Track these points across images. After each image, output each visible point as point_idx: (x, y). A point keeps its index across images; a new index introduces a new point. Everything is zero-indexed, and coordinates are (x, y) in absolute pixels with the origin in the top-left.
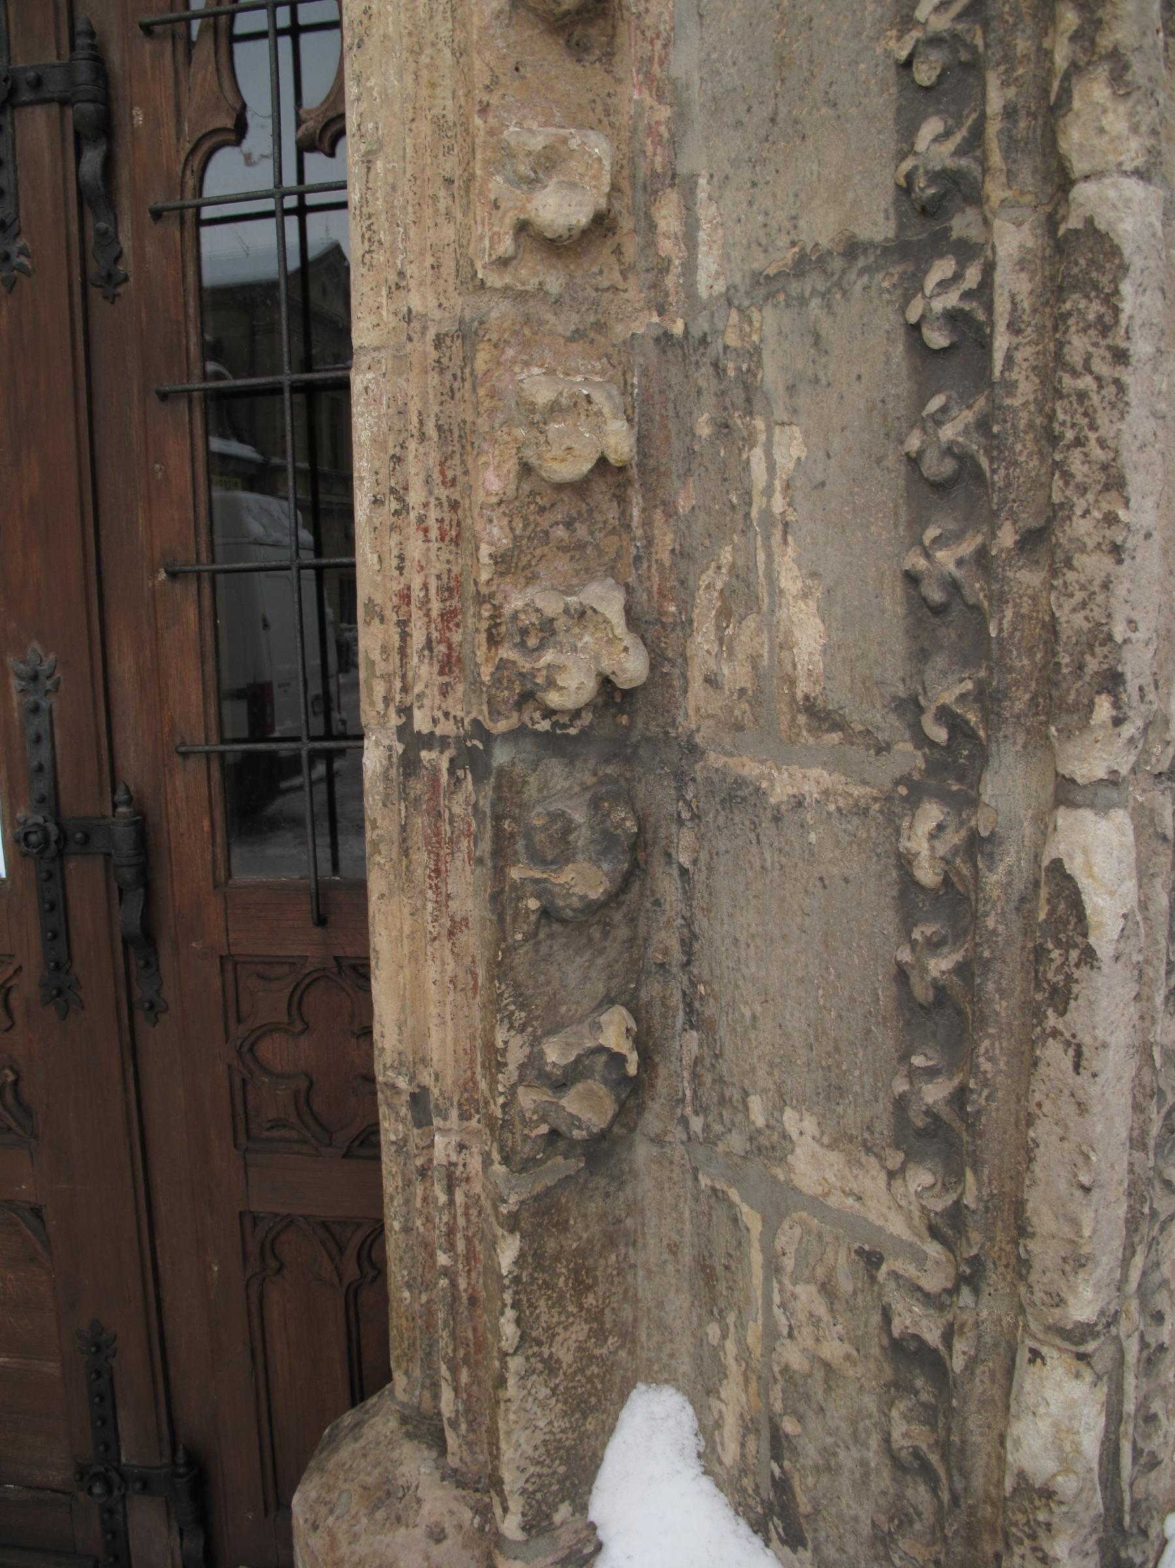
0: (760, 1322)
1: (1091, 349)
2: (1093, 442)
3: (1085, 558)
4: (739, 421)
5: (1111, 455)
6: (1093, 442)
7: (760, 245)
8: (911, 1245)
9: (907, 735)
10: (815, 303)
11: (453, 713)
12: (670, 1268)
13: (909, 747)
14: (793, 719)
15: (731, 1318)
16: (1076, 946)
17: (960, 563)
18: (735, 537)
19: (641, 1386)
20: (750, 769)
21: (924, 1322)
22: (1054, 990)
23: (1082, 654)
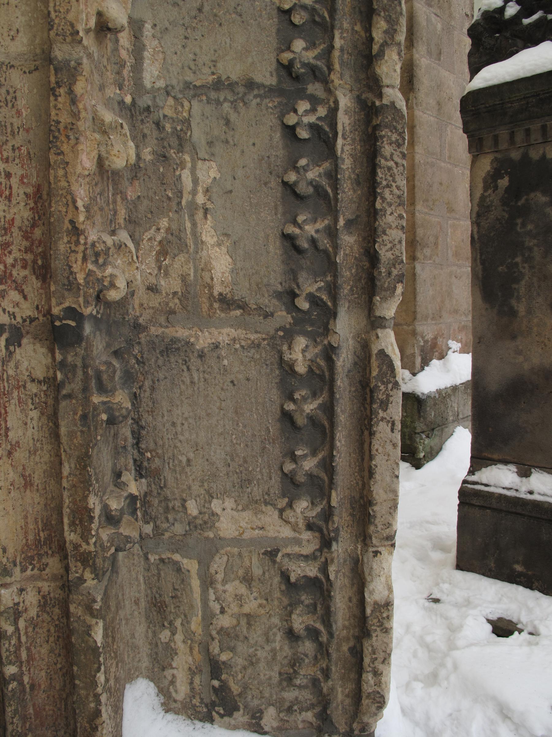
0: (200, 615)
1: (393, 151)
2: (394, 187)
3: (391, 231)
4: (174, 155)
5: (402, 193)
6: (394, 187)
7: (190, 69)
8: (294, 538)
9: (283, 308)
10: (226, 105)
11: (7, 310)
12: (136, 613)
13: (284, 313)
14: (211, 305)
15: (178, 623)
16: (391, 382)
17: (317, 231)
18: (171, 214)
19: (127, 686)
20: (181, 333)
21: (307, 568)
22: (382, 402)
23: (390, 268)
